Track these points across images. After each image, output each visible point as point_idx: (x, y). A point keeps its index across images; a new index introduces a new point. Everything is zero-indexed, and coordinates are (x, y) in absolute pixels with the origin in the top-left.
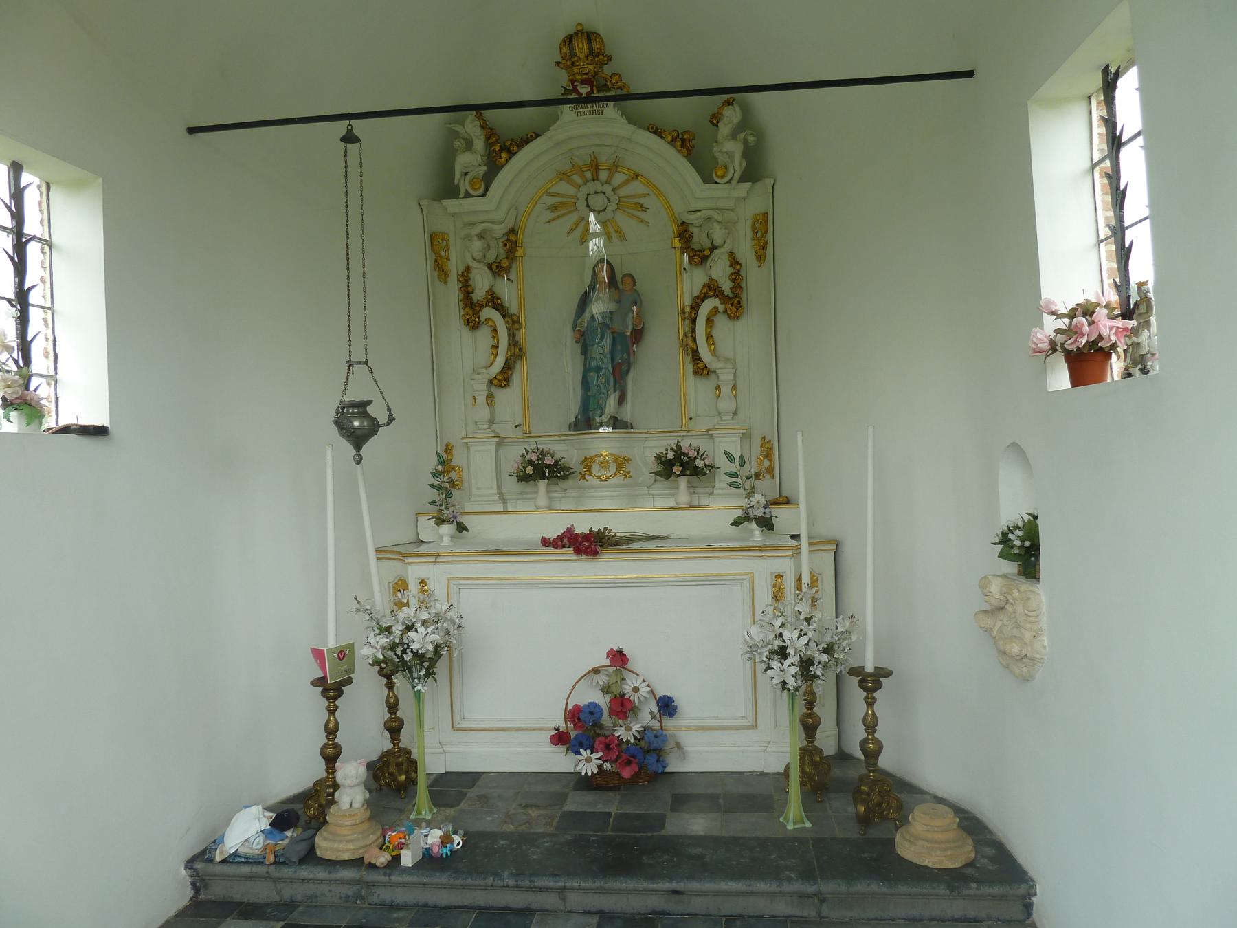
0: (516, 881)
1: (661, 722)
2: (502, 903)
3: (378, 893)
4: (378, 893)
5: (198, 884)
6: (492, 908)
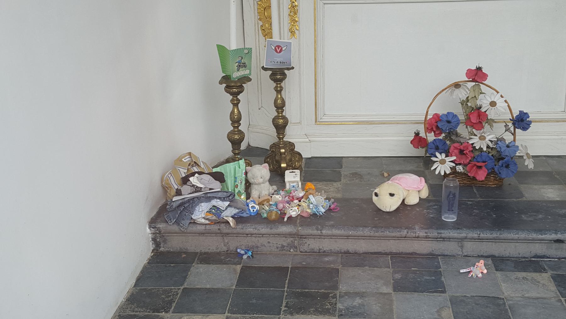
0: (426, 233)
2: (411, 250)
3: (308, 243)
4: (308, 243)
5: (158, 240)
6: (401, 253)
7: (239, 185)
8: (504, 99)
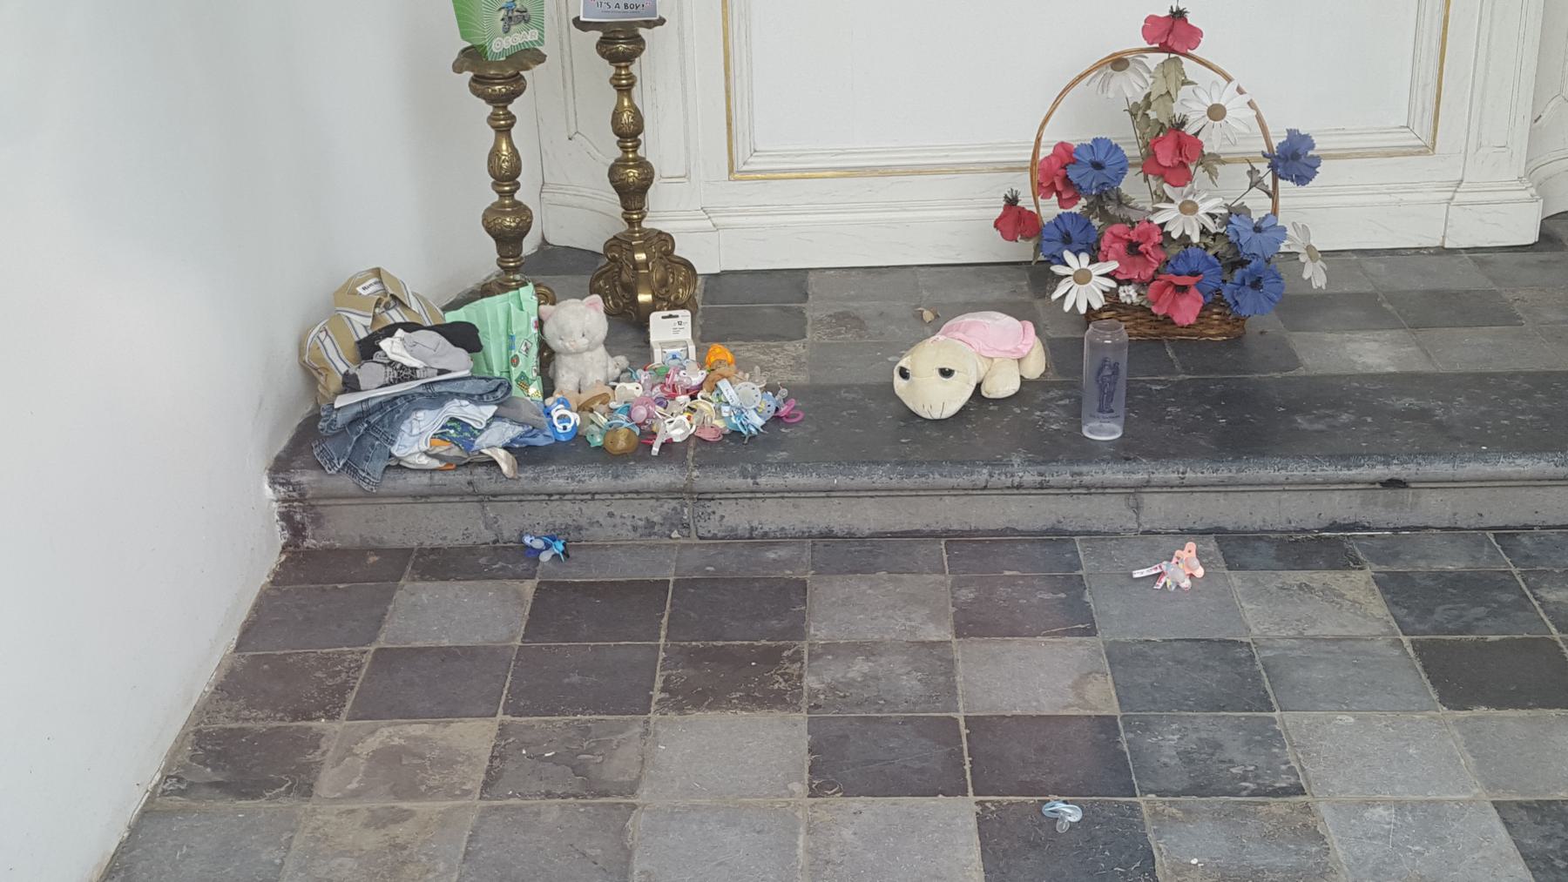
1: (1273, 195)
2: (999, 523)
3: (720, 512)
4: (720, 512)
5: (298, 517)
7: (521, 357)
8: (1245, 98)
